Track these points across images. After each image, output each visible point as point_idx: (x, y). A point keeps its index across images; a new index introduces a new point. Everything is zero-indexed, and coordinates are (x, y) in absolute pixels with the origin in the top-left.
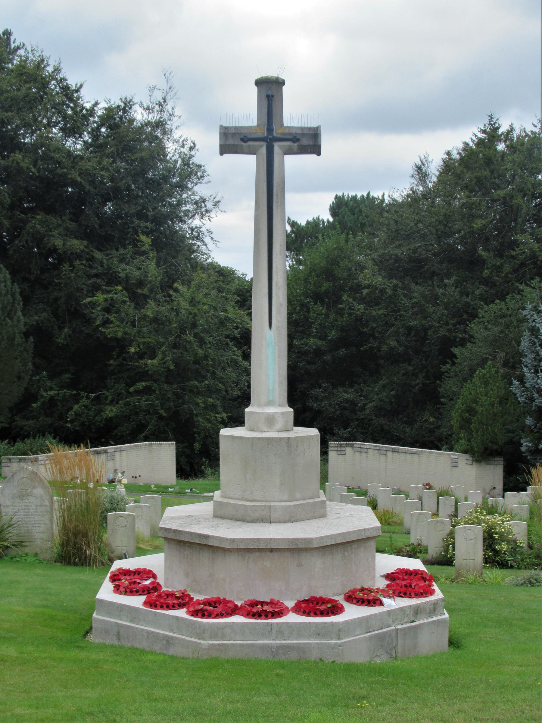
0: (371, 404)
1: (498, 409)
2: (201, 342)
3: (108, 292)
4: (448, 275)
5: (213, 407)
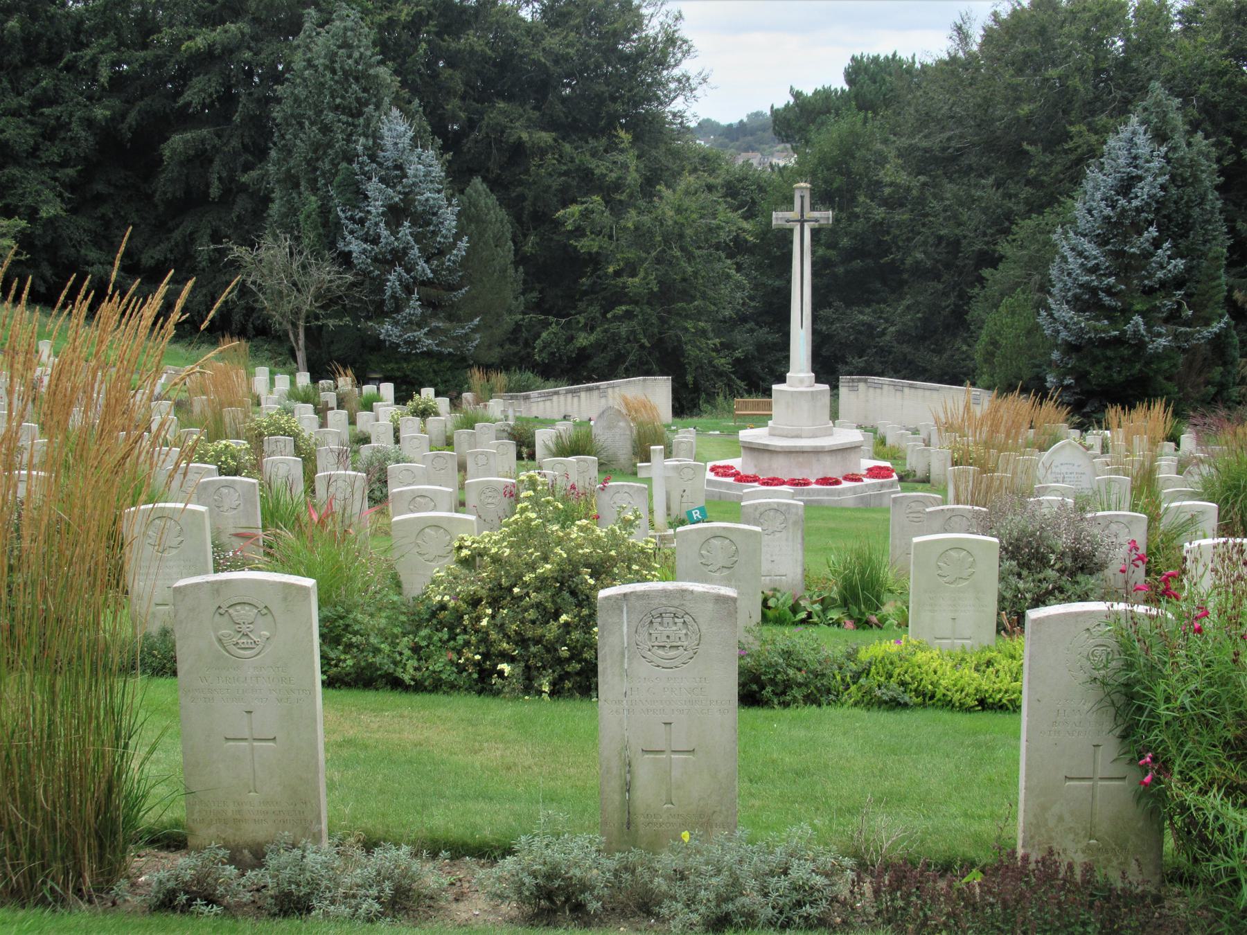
0: (892, 329)
1: (1023, 341)
2: (690, 257)
3: (583, 203)
4: (988, 171)
5: (703, 332)
